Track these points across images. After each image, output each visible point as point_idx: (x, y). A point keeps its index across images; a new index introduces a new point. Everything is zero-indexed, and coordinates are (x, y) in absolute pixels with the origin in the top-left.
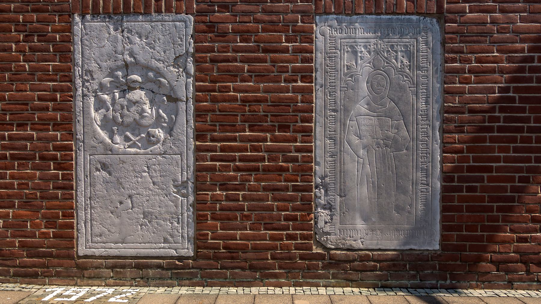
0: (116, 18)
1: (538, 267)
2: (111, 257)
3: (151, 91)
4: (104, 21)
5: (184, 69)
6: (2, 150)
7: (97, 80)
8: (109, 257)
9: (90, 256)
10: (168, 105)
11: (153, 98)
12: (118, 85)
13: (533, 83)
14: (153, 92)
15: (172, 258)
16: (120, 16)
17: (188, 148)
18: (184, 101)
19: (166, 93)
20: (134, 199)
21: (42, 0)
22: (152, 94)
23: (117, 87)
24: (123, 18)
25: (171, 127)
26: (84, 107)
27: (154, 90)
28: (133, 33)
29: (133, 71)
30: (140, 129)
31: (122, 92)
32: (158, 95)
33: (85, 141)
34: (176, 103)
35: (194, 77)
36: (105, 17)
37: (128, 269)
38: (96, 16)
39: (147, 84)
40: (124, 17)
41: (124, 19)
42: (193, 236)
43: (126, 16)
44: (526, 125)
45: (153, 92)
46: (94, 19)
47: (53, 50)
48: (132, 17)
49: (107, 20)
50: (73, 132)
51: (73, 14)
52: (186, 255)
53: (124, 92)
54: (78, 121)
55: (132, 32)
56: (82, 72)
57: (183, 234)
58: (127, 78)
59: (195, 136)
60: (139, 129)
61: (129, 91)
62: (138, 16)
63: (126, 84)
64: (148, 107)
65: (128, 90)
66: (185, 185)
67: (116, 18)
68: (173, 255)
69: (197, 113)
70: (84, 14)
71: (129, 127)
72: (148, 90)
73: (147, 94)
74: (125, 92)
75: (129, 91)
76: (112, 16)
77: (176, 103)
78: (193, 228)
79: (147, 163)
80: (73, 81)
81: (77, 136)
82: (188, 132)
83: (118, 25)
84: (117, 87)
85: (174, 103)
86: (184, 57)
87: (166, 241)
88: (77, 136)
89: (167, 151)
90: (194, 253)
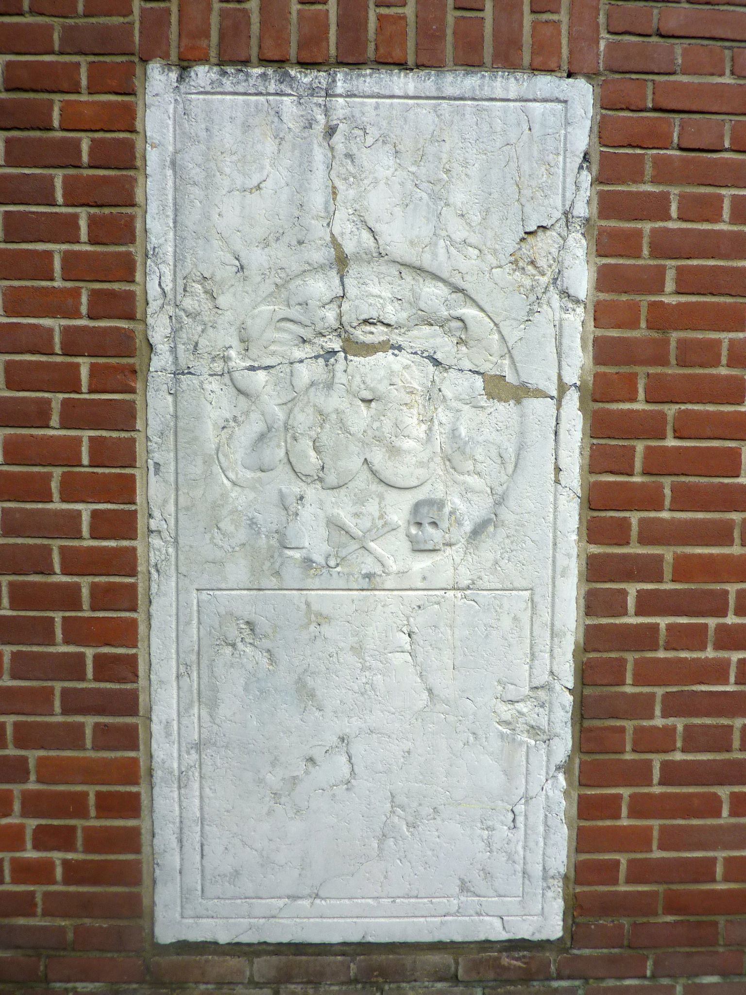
0: (306, 80)
1: (179, 942)
2: (271, 948)
3: (429, 357)
4: (261, 89)
5: (555, 280)
6: (4, 536)
7: (229, 313)
8: (264, 947)
9: (447, 943)
10: (489, 410)
11: (433, 381)
12: (307, 333)
13: (628, 543)
14: (436, 363)
15: (486, 945)
16: (321, 74)
17: (559, 570)
18: (552, 398)
19: (485, 367)
20: (358, 748)
21: (26, 6)
22: (431, 368)
23: (304, 341)
24: (334, 81)
25: (500, 490)
26: (180, 414)
27: (439, 356)
28: (370, 140)
29: (364, 284)
30: (386, 495)
31: (321, 361)
32: (453, 373)
33: (181, 541)
34: (518, 402)
35: (591, 308)
36: (264, 76)
37: (331, 985)
38: (230, 70)
39: (415, 332)
40: (340, 76)
41: (339, 84)
42: (563, 870)
43: (346, 74)
44: (712, 622)
45: (436, 363)
46: (224, 80)
47: (64, 196)
48: (368, 79)
49: (272, 87)
50: (138, 508)
51: (145, 61)
52: (537, 937)
53: (327, 361)
54: (157, 465)
55: (366, 133)
56: (174, 280)
57: (529, 868)
58: (340, 307)
59: (585, 524)
60: (381, 497)
61: (350, 357)
62: (391, 75)
63: (340, 330)
64: (415, 418)
65: (342, 354)
66: (542, 694)
67: (306, 80)
68: (493, 938)
69: (595, 441)
70: (185, 64)
71: (343, 491)
72: (416, 353)
73: (414, 368)
74: (332, 360)
75: (350, 357)
76: (292, 73)
77: (518, 402)
78: (566, 844)
79: (408, 620)
80: (138, 316)
81: (152, 521)
82: (561, 508)
83: (315, 109)
84: (304, 341)
85: (512, 402)
86: (554, 234)
87: (464, 888)
88: (152, 521)
89: (480, 578)
90: (565, 928)
